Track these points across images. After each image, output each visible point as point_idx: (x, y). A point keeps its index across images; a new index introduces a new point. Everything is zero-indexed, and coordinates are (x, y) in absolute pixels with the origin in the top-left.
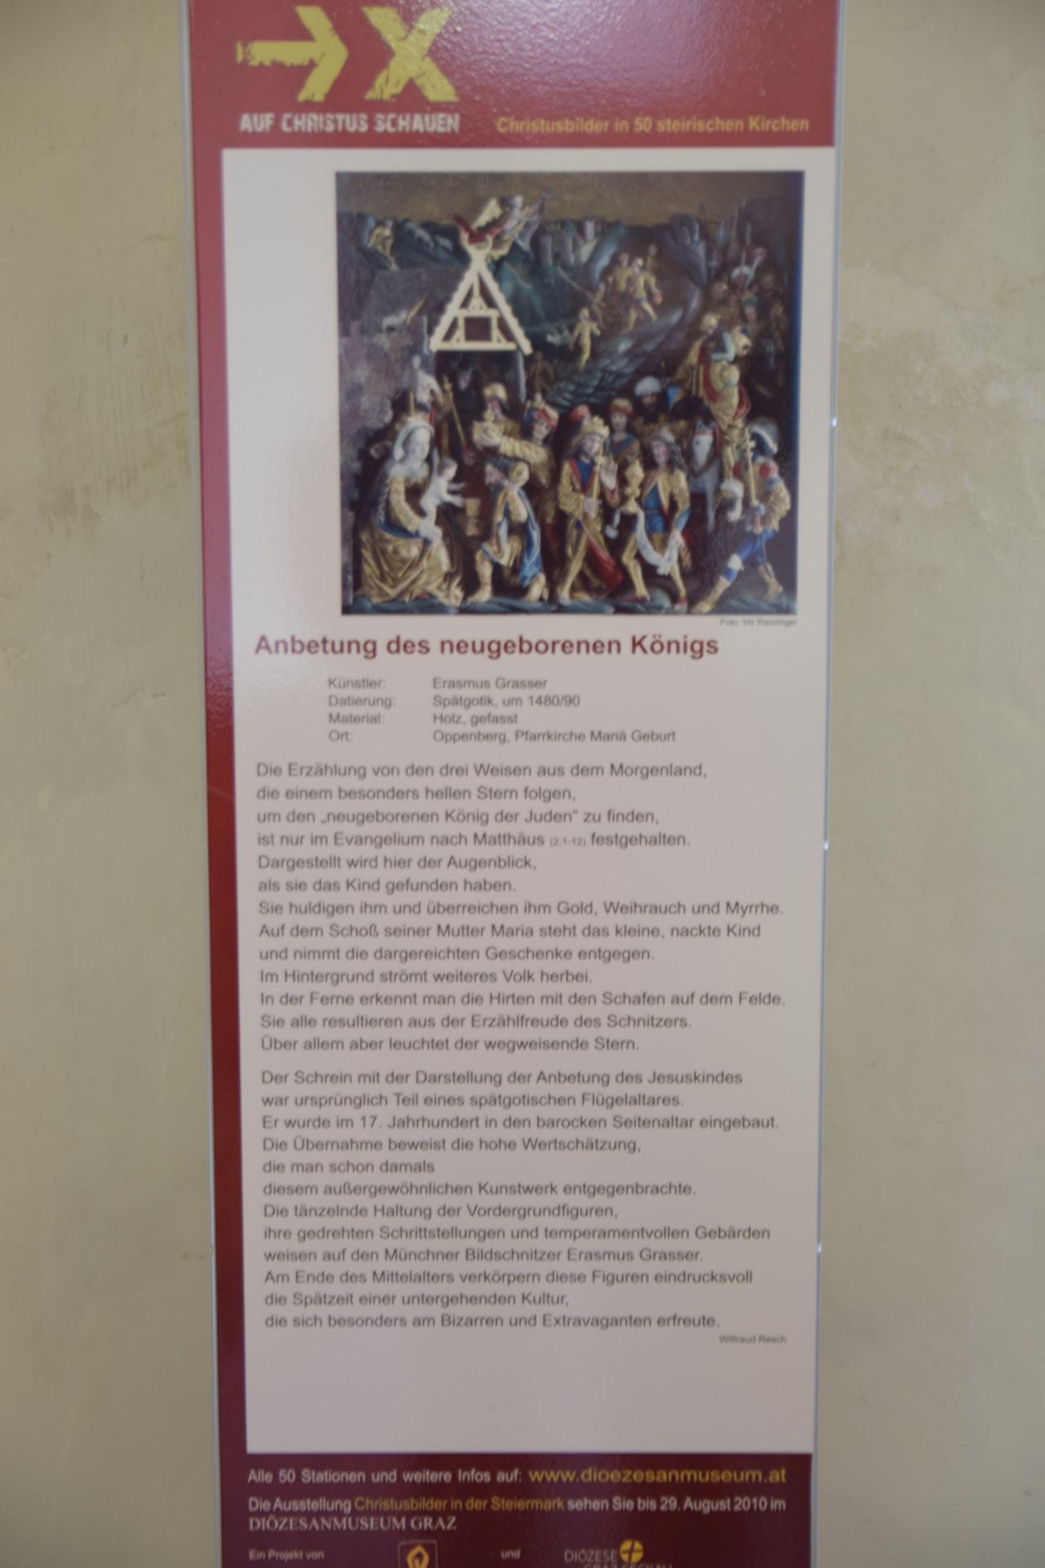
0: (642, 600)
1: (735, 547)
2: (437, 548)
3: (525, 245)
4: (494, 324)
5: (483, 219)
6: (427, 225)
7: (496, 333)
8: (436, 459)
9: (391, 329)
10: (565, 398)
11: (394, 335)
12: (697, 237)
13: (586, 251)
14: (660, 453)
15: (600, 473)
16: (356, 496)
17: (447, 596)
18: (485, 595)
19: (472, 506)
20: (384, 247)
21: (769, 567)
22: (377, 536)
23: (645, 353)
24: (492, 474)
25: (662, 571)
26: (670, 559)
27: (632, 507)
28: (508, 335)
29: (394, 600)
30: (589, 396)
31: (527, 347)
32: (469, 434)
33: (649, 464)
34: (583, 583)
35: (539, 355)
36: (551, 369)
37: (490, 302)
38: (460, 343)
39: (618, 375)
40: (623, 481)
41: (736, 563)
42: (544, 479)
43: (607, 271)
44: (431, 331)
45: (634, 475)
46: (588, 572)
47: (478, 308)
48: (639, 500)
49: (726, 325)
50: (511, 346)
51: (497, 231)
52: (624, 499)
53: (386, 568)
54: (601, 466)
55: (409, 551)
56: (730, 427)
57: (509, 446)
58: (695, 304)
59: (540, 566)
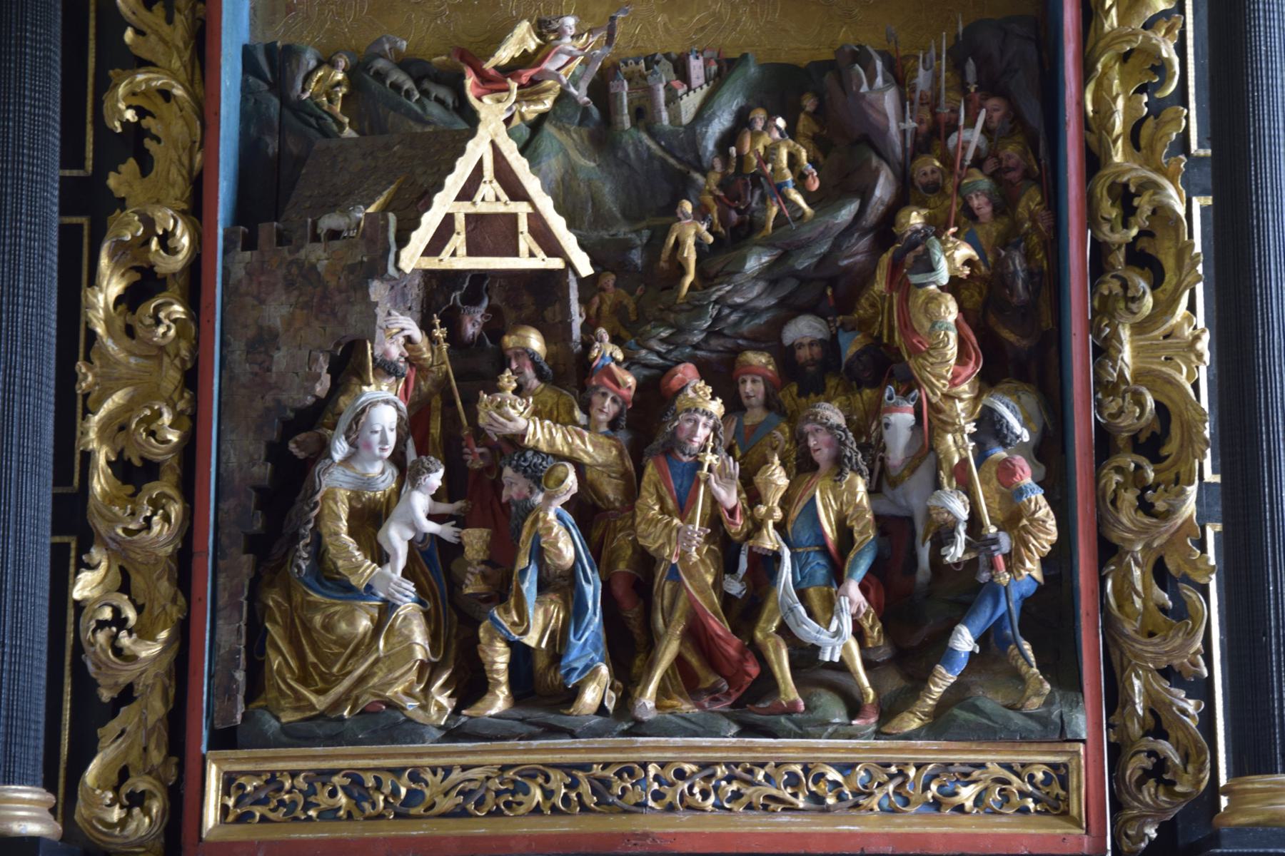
0: (791, 709)
1: (962, 613)
2: (405, 618)
3: (581, 94)
4: (523, 225)
5: (505, 54)
6: (405, 64)
7: (526, 241)
8: (411, 455)
9: (334, 234)
10: (651, 350)
11: (337, 244)
12: (879, 81)
13: (690, 104)
14: (820, 445)
15: (707, 482)
16: (258, 525)
17: (424, 707)
18: (499, 701)
19: (475, 540)
20: (330, 101)
21: (1027, 647)
22: (297, 598)
23: (795, 274)
24: (514, 485)
25: (830, 654)
26: (838, 633)
27: (770, 540)
28: (551, 246)
29: (322, 715)
30: (696, 347)
31: (585, 267)
32: (473, 415)
33: (802, 466)
34: (682, 673)
35: (610, 279)
36: (630, 303)
37: (516, 191)
38: (457, 258)
39: (749, 311)
40: (753, 496)
41: (964, 641)
42: (611, 490)
43: (730, 138)
44: (403, 241)
45: (769, 483)
46: (694, 661)
47: (490, 199)
48: (779, 527)
49: (936, 226)
50: (557, 263)
51: (526, 75)
52: (757, 526)
53: (311, 658)
54: (710, 470)
55: (352, 622)
56: (949, 397)
57: (539, 433)
58: (883, 190)
59: (603, 649)
